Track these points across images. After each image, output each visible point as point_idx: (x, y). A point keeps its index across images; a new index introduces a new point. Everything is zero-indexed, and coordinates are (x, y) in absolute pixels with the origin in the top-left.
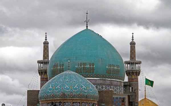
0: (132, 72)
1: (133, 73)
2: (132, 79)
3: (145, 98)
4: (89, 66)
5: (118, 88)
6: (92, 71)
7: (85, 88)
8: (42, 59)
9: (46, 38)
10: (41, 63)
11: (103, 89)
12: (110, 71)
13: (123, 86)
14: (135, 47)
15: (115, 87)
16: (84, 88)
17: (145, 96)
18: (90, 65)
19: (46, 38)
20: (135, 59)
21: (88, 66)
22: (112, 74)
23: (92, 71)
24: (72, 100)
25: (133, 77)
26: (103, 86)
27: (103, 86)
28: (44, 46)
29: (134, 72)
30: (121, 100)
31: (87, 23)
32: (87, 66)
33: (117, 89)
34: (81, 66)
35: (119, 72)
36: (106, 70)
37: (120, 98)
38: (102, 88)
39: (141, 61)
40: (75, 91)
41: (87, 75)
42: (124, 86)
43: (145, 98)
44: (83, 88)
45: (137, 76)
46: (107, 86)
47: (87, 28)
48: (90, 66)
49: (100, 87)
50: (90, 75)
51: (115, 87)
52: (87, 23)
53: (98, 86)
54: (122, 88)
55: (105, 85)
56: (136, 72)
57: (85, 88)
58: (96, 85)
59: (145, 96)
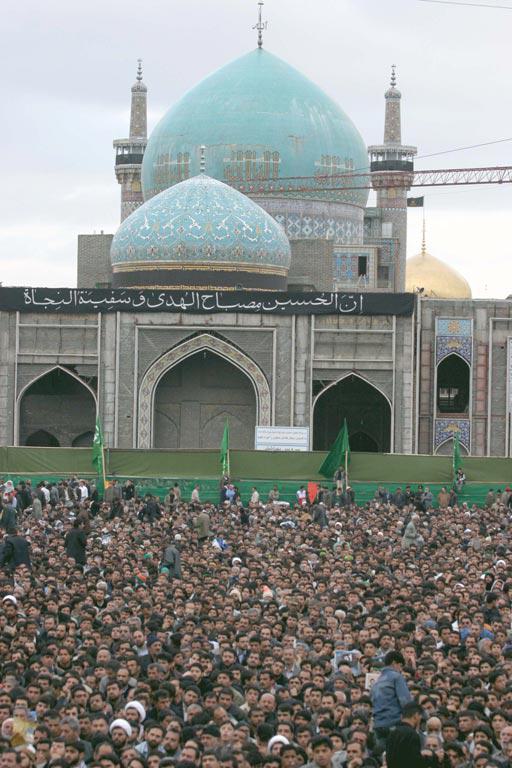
4: (175, 162)
5: (349, 225)
15: (294, 219)
16: (248, 231)
18: (267, 155)
19: (393, 74)
21: (260, 160)
27: (305, 219)
29: (128, 171)
33: (346, 228)
34: (328, 164)
42: (365, 218)
48: (267, 158)
57: (200, 227)
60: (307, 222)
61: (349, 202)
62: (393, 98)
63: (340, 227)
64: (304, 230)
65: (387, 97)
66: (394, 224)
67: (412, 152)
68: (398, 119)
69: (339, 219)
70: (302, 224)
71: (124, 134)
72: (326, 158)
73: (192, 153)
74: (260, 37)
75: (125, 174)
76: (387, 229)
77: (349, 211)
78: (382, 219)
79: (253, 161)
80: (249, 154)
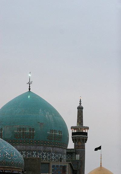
0: (78, 138)
1: (84, 139)
2: (78, 146)
3: (101, 166)
4: (16, 131)
5: (60, 155)
6: (31, 137)
7: (9, 155)
8: (76, 125)
9: (80, 102)
10: (75, 129)
11: (33, 156)
12: (52, 137)
13: (66, 153)
14: (82, 111)
15: (57, 154)
16: (8, 155)
17: (101, 164)
18: (30, 129)
19: (80, 102)
20: (83, 125)
21: (28, 131)
22: (22, 139)
23: (31, 137)
24: (4, 167)
25: (80, 144)
26: (33, 152)
27: (33, 152)
28: (78, 111)
29: (80, 138)
30: (62, 169)
31: (30, 85)
32: (57, 134)
33: (59, 156)
34: (52, 133)
35: (61, 138)
36: (15, 135)
37: (61, 166)
38: (33, 154)
39: (89, 127)
40: (15, 159)
41: (26, 140)
42: (67, 153)
43: (101, 166)
44: (6, 155)
45: (84, 143)
46: (39, 152)
47: (29, 91)
48: (30, 131)
49: (39, 154)
50: (26, 140)
51: (57, 154)
52: (30, 85)
53: (38, 153)
54: (65, 156)
55: (36, 151)
56: (83, 139)
57: (9, 155)
58: (36, 152)
59: (101, 164)
60: (53, 154)
61: (64, 147)
62: (80, 109)
63: (57, 156)
64: (52, 157)
65: (78, 109)
66: (80, 155)
67: (88, 128)
68: (82, 116)
69: (56, 153)
70: (43, 154)
71: (75, 124)
72: (52, 131)
73: (3, 129)
74: (30, 87)
75: (76, 139)
76: (78, 157)
77: (61, 150)
78: (76, 153)
79: (25, 131)
80: (23, 129)
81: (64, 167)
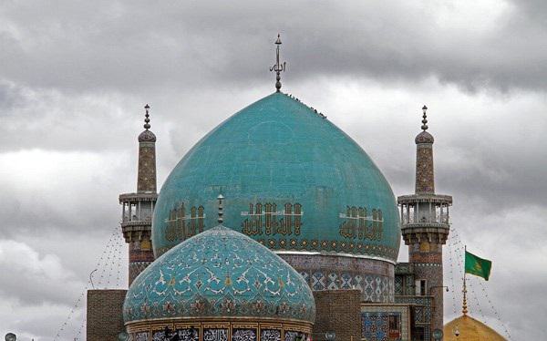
0: (421, 230)
1: (426, 233)
2: (423, 255)
3: (465, 316)
4: (283, 213)
5: (379, 282)
6: (293, 229)
7: (273, 283)
8: (135, 191)
9: (147, 121)
10: (131, 203)
11: (330, 288)
12: (353, 227)
13: (393, 276)
14: (431, 150)
15: (369, 280)
16: (269, 283)
17: (465, 308)
18: (288, 208)
19: (147, 121)
20: (433, 191)
21: (282, 213)
22: (357, 239)
23: (293, 229)
24: (229, 320)
25: (427, 248)
26: (330, 276)
27: (330, 276)
28: (141, 149)
29: (427, 230)
30: (386, 323)
31: (278, 74)
32: (277, 213)
33: (375, 285)
34: (258, 211)
35: (380, 231)
36: (340, 226)
37: (385, 315)
38: (328, 282)
39: (451, 197)
40: (241, 293)
41: (277, 240)
42: (396, 275)
43: (465, 316)
44: (265, 282)
45: (439, 245)
46: (344, 275)
47: (278, 91)
48: (288, 211)
49: (321, 281)
50: (288, 240)
51: (369, 280)
52: (278, 74)
53: (313, 277)
54: (391, 284)
55: (337, 273)
56: (435, 233)
57: (273, 283)
58: (306, 275)
59: (465, 308)
81: (394, 322)
